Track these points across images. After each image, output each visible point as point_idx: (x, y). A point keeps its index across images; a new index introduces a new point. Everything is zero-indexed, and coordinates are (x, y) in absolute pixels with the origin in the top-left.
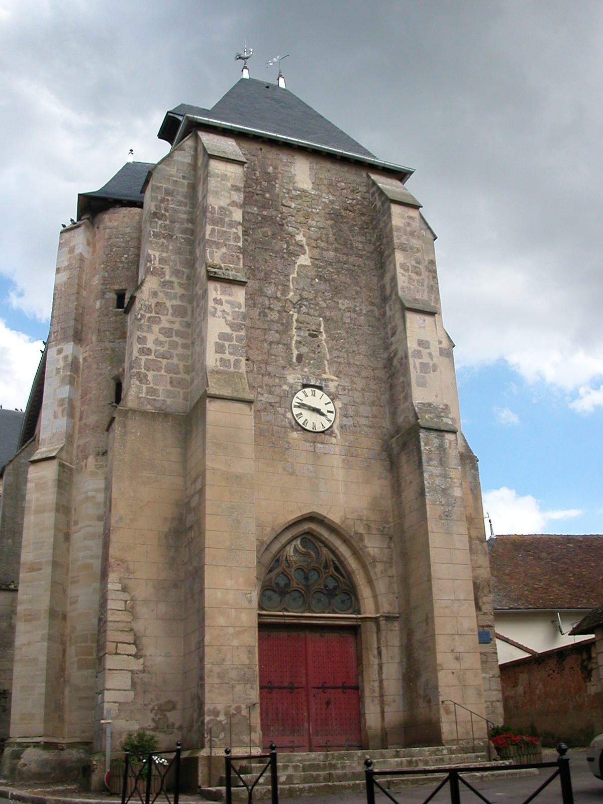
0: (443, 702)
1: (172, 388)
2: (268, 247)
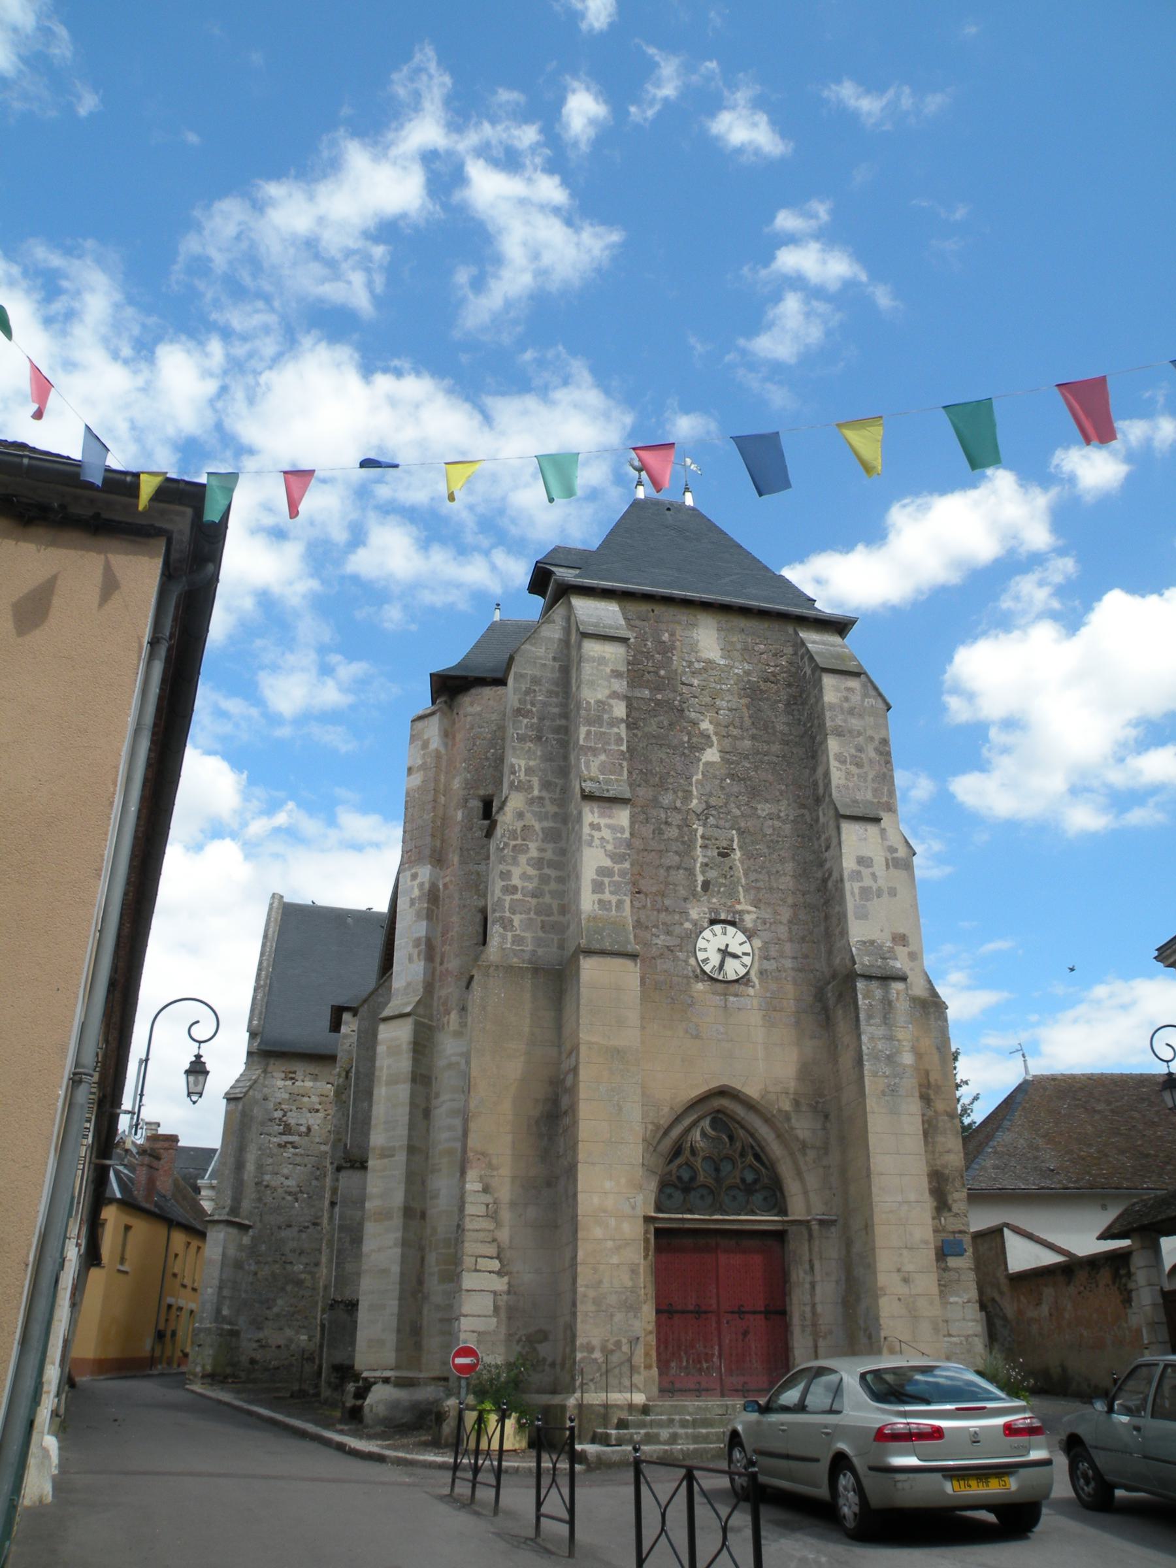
0: (885, 1338)
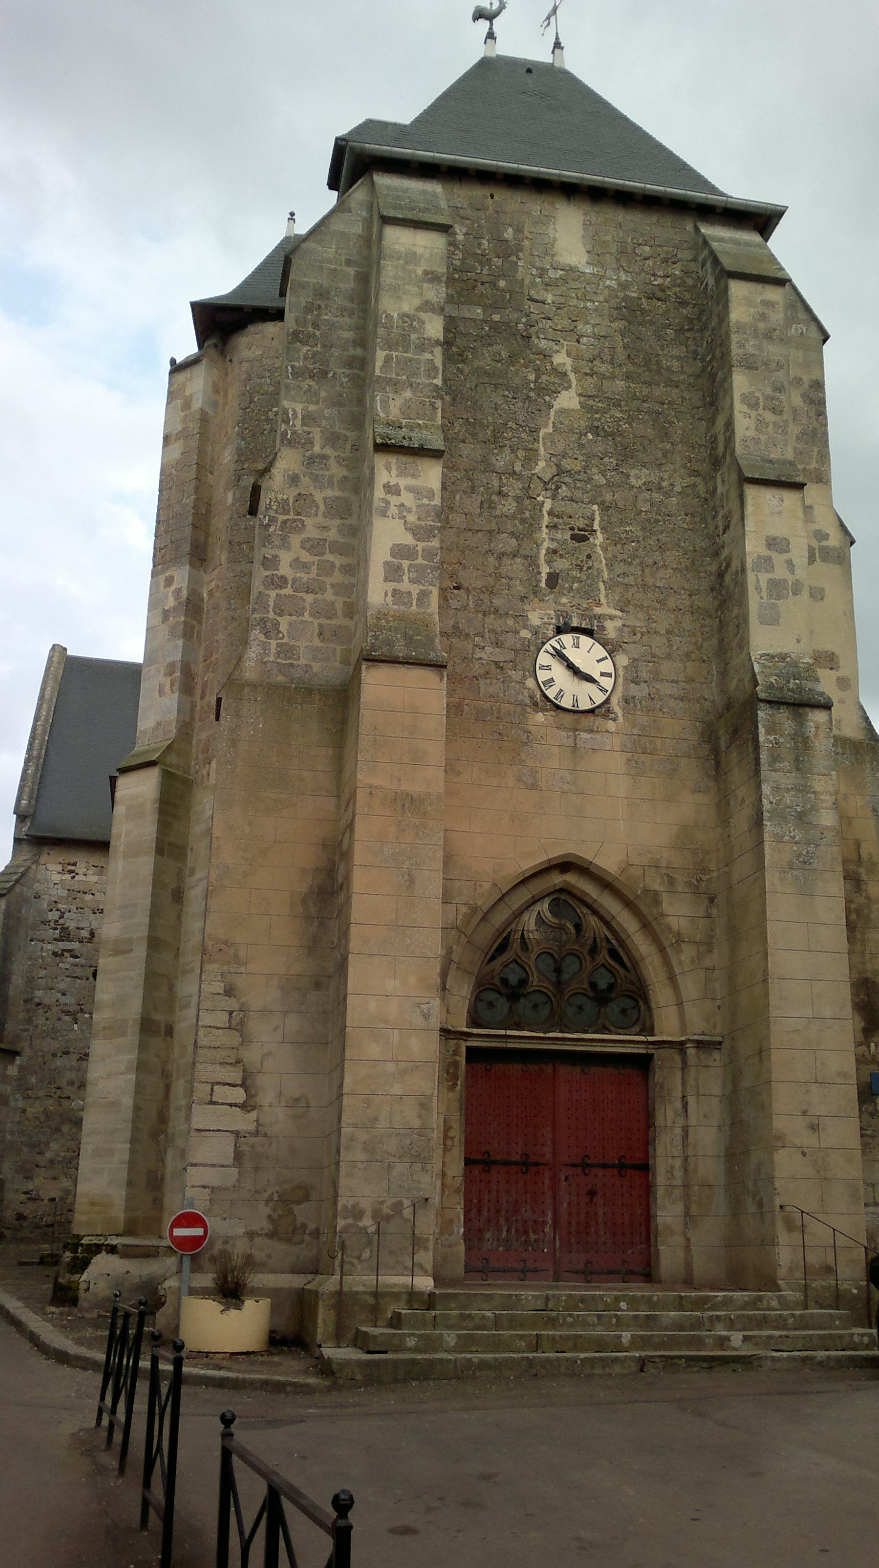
0: (781, 1207)
1: (322, 644)
2: (500, 381)
